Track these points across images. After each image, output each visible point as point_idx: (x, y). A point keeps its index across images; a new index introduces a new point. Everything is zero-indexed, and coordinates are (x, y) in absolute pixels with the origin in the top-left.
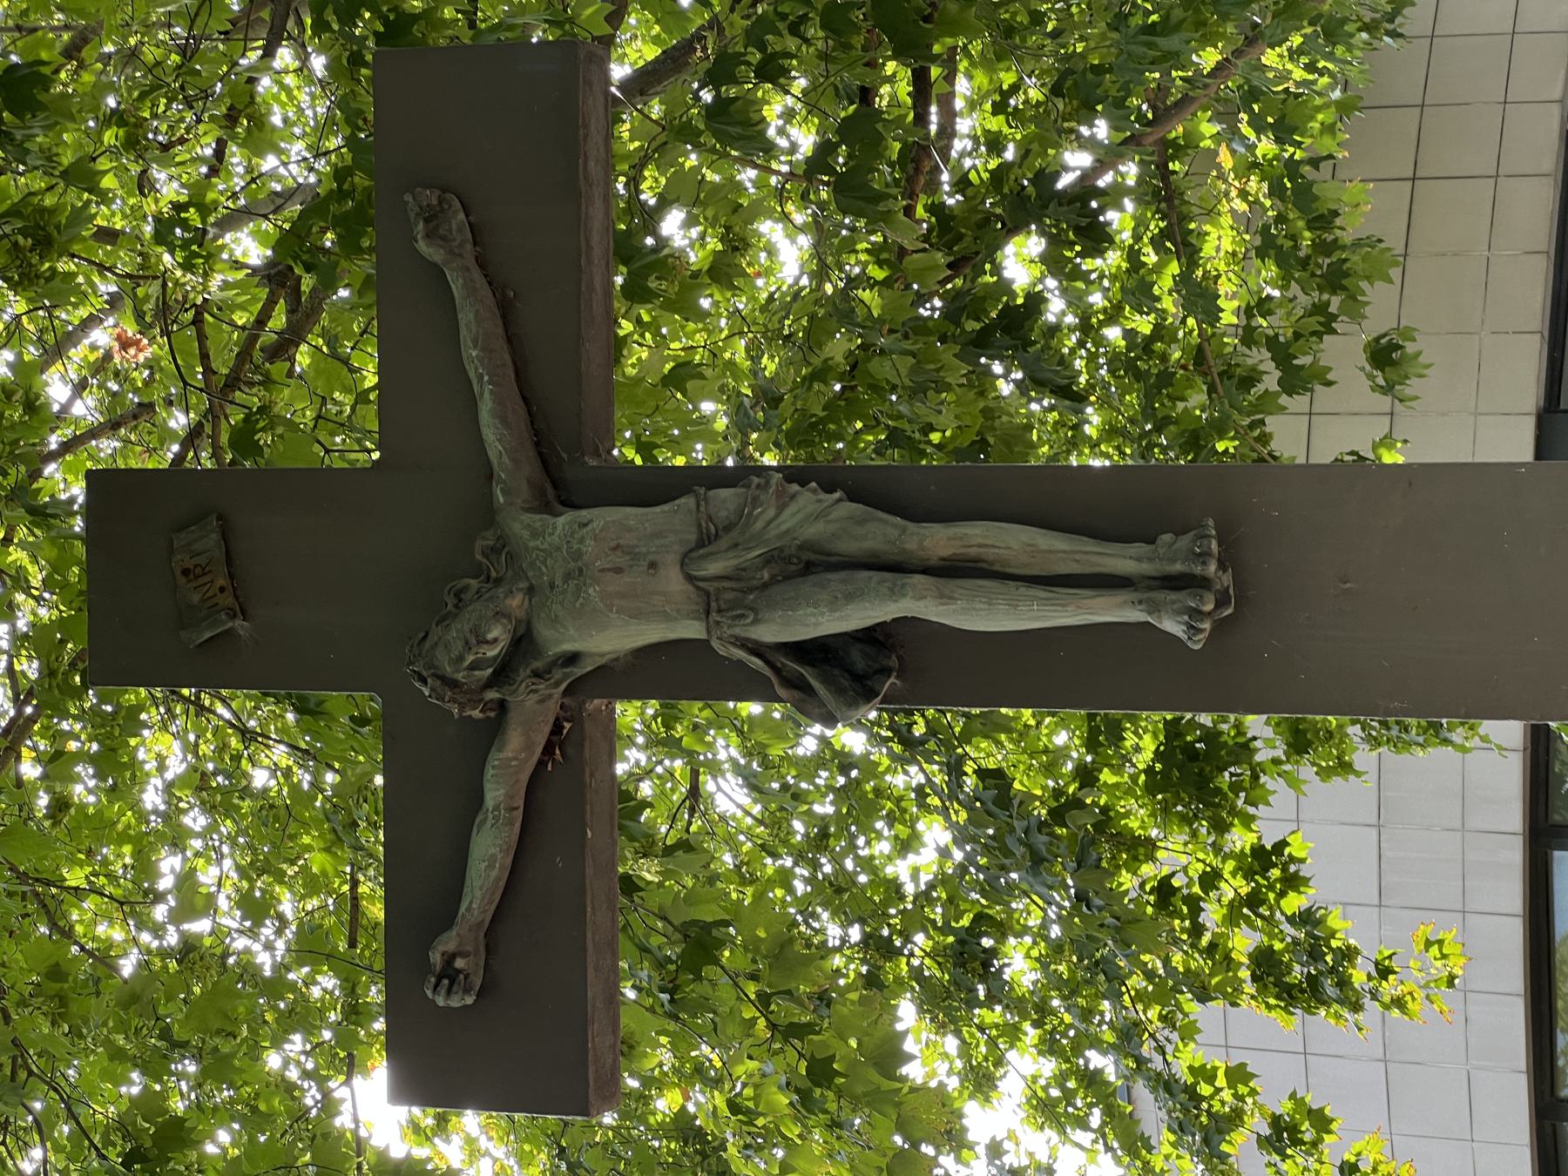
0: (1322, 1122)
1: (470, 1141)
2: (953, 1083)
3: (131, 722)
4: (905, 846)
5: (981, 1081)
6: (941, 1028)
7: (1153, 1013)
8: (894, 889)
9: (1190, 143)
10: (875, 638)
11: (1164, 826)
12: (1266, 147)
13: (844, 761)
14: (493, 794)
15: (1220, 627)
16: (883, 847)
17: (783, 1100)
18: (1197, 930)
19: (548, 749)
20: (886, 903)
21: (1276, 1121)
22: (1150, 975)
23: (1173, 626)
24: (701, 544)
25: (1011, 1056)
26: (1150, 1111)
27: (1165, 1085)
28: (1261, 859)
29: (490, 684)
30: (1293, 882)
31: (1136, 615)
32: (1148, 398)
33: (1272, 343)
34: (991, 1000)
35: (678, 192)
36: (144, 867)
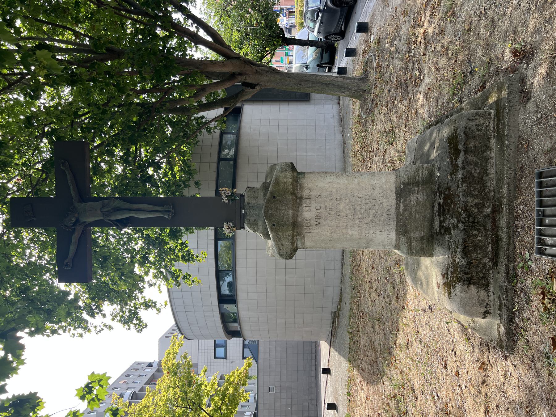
0: (190, 276)
1: (75, 286)
2: (143, 274)
3: (20, 232)
4: (136, 244)
5: (147, 274)
6: (141, 267)
7: (169, 263)
8: (135, 249)
9: (172, 157)
10: (127, 219)
11: (170, 240)
12: (182, 158)
13: (128, 234)
14: (73, 241)
15: (172, 217)
16: (133, 244)
17: (117, 278)
18: (174, 253)
19: (81, 235)
20: (134, 252)
21: (184, 276)
22: (169, 259)
23: (166, 217)
24: (103, 207)
25: (151, 270)
26: (169, 276)
27: (170, 272)
28: (182, 244)
29: (72, 226)
30: (187, 247)
31: (162, 215)
32: (167, 188)
33: (183, 181)
34: (147, 263)
35: (103, 161)
36: (24, 252)
